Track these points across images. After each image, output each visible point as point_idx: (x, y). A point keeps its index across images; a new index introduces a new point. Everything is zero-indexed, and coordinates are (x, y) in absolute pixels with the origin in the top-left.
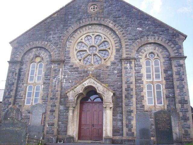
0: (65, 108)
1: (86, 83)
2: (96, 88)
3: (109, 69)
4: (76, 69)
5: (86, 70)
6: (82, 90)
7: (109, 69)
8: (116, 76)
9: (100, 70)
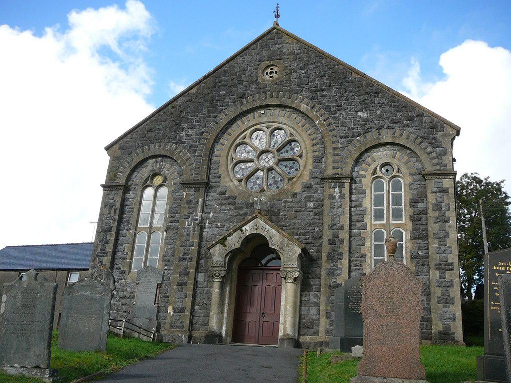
0: (207, 279)
1: (248, 229)
2: (268, 239)
3: (297, 200)
4: (230, 200)
5: (251, 201)
6: (240, 242)
7: (297, 200)
8: (311, 214)
9: (280, 200)
